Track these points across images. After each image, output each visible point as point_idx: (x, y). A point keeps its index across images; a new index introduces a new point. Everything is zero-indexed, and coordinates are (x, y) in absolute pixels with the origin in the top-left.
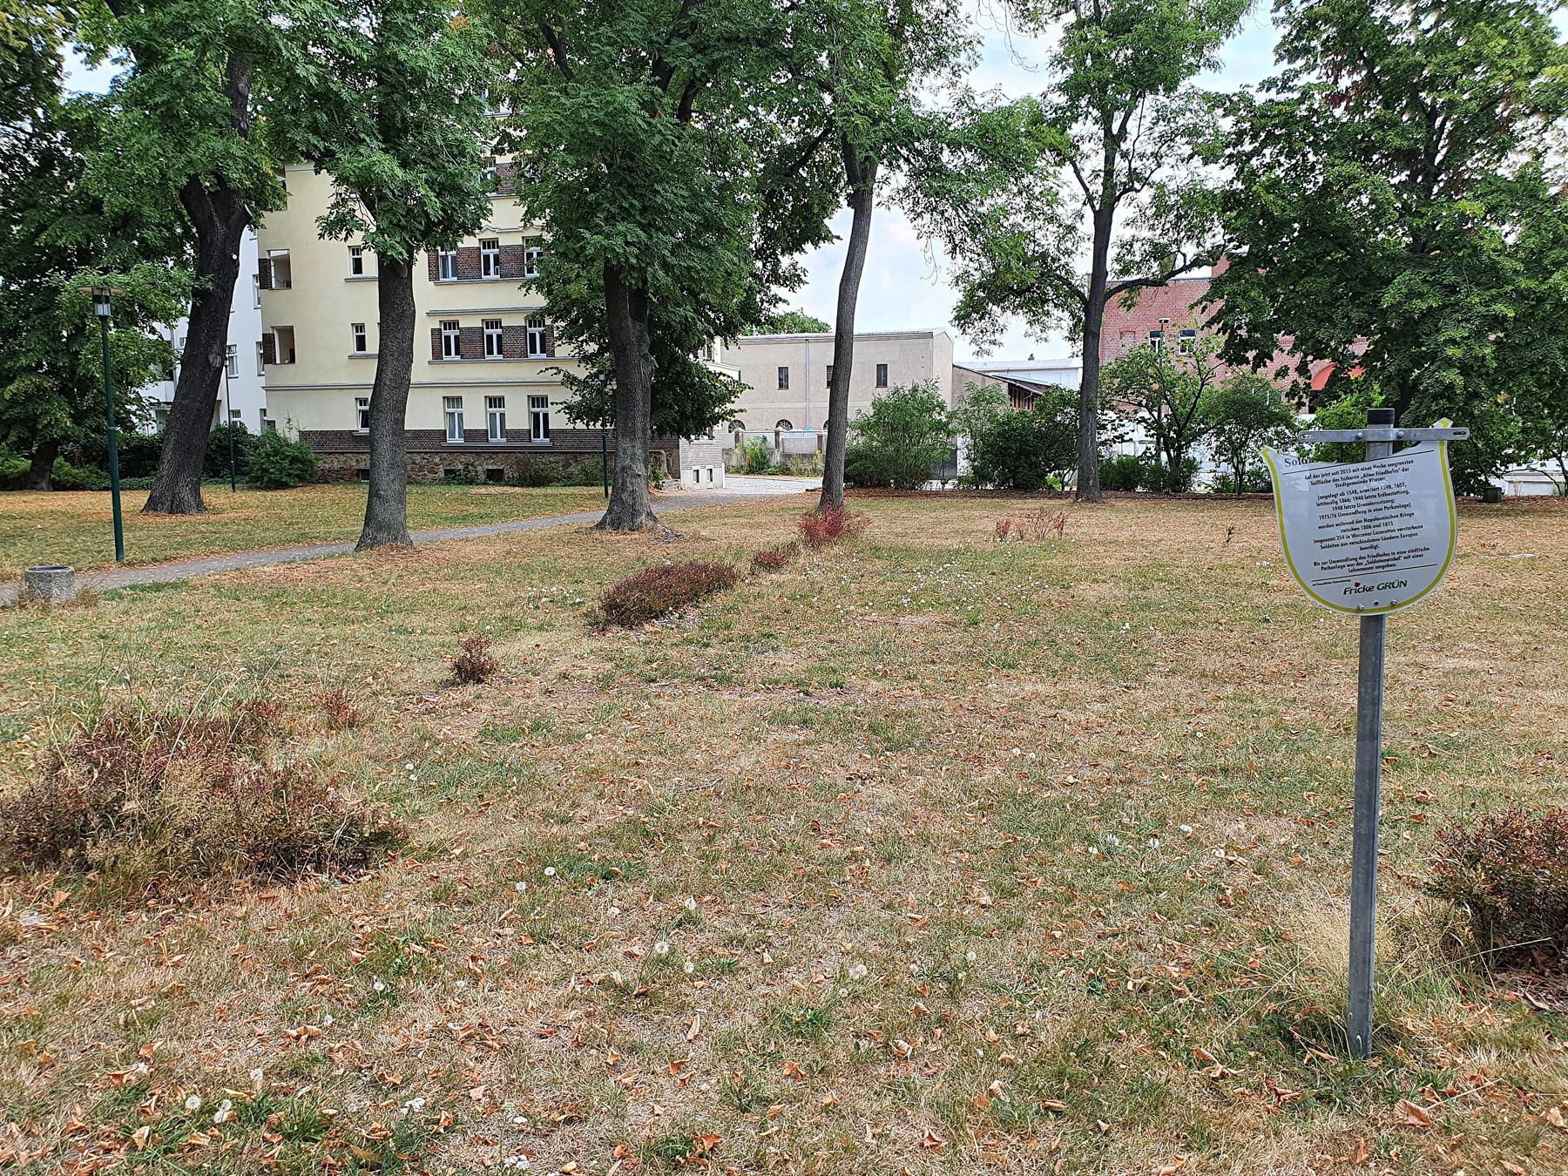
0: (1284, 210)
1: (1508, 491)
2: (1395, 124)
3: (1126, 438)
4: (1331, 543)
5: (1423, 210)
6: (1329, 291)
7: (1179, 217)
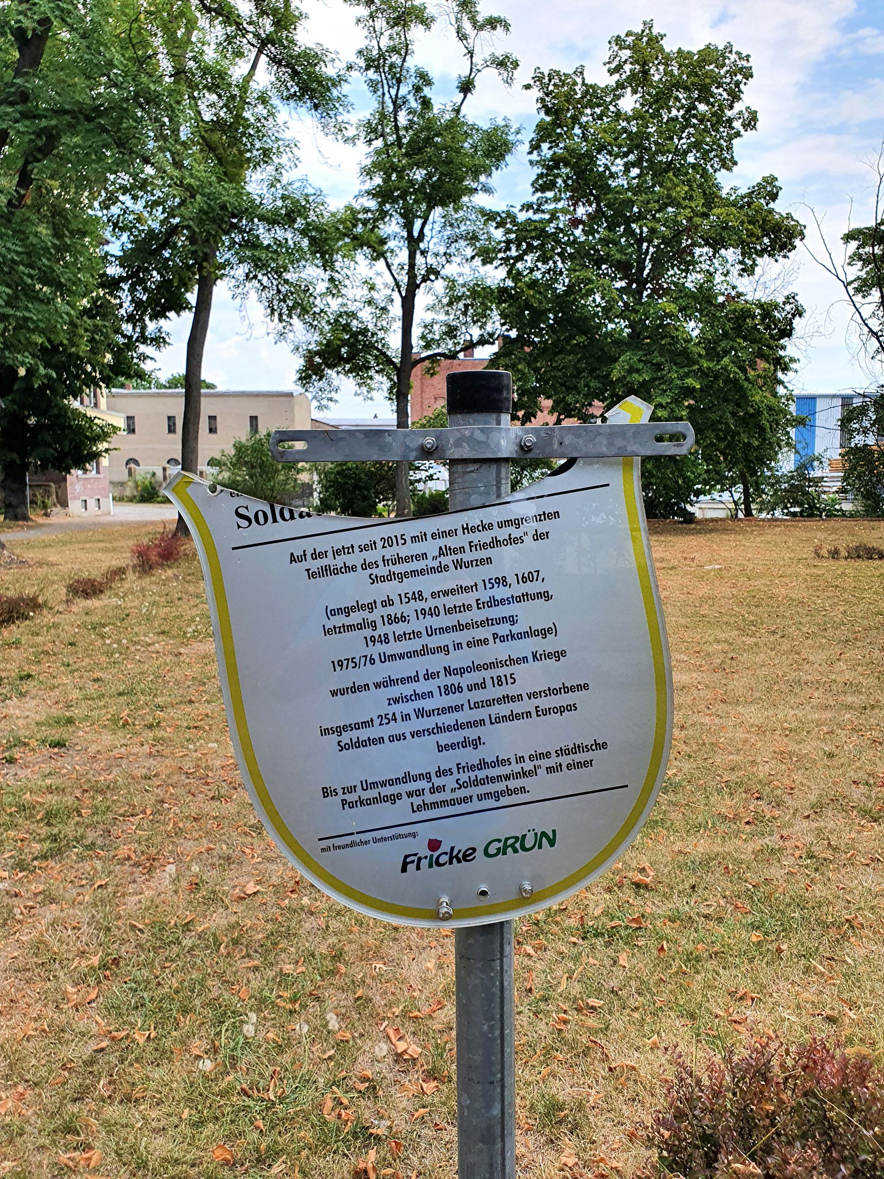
0: (541, 303)
1: (699, 515)
2: (616, 243)
3: (435, 477)
4: (364, 734)
5: (637, 307)
6: (575, 367)
7: (466, 306)
